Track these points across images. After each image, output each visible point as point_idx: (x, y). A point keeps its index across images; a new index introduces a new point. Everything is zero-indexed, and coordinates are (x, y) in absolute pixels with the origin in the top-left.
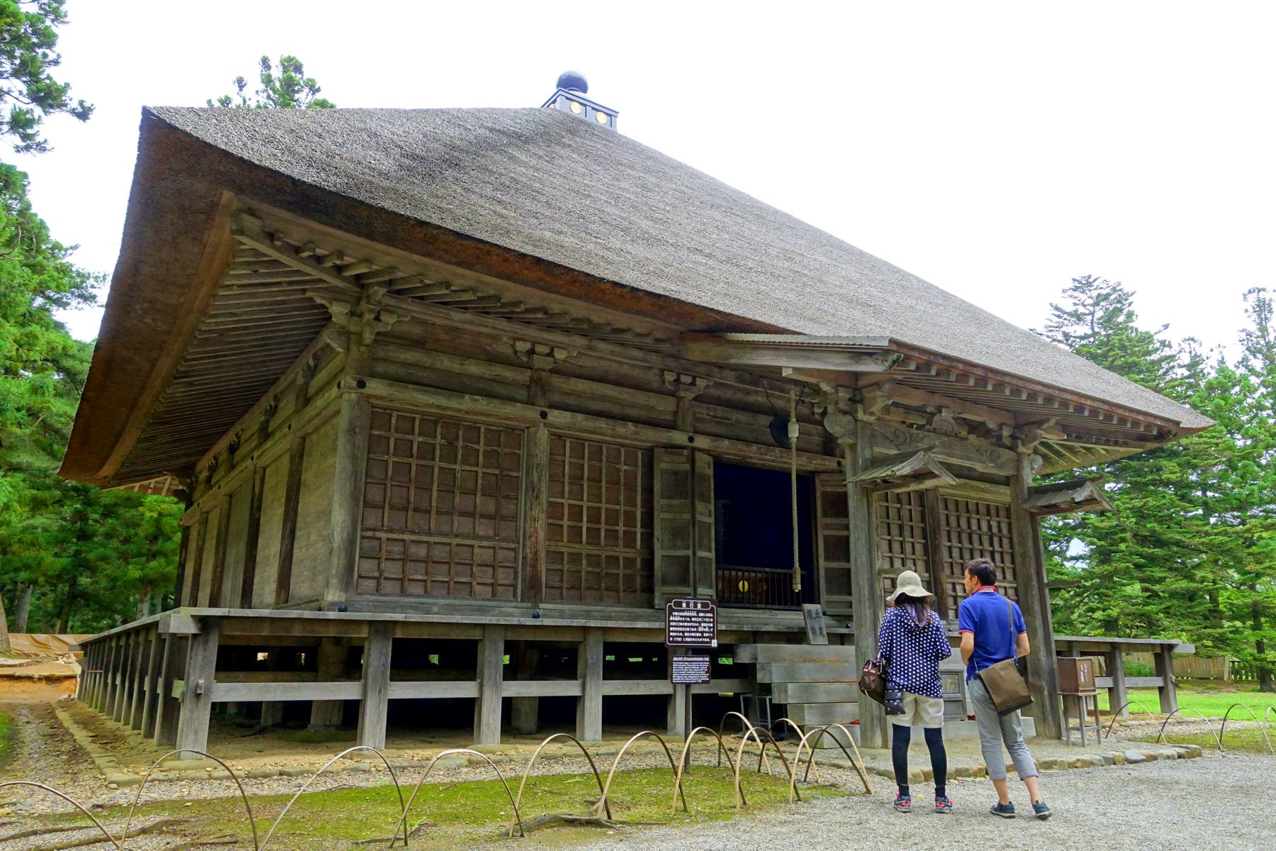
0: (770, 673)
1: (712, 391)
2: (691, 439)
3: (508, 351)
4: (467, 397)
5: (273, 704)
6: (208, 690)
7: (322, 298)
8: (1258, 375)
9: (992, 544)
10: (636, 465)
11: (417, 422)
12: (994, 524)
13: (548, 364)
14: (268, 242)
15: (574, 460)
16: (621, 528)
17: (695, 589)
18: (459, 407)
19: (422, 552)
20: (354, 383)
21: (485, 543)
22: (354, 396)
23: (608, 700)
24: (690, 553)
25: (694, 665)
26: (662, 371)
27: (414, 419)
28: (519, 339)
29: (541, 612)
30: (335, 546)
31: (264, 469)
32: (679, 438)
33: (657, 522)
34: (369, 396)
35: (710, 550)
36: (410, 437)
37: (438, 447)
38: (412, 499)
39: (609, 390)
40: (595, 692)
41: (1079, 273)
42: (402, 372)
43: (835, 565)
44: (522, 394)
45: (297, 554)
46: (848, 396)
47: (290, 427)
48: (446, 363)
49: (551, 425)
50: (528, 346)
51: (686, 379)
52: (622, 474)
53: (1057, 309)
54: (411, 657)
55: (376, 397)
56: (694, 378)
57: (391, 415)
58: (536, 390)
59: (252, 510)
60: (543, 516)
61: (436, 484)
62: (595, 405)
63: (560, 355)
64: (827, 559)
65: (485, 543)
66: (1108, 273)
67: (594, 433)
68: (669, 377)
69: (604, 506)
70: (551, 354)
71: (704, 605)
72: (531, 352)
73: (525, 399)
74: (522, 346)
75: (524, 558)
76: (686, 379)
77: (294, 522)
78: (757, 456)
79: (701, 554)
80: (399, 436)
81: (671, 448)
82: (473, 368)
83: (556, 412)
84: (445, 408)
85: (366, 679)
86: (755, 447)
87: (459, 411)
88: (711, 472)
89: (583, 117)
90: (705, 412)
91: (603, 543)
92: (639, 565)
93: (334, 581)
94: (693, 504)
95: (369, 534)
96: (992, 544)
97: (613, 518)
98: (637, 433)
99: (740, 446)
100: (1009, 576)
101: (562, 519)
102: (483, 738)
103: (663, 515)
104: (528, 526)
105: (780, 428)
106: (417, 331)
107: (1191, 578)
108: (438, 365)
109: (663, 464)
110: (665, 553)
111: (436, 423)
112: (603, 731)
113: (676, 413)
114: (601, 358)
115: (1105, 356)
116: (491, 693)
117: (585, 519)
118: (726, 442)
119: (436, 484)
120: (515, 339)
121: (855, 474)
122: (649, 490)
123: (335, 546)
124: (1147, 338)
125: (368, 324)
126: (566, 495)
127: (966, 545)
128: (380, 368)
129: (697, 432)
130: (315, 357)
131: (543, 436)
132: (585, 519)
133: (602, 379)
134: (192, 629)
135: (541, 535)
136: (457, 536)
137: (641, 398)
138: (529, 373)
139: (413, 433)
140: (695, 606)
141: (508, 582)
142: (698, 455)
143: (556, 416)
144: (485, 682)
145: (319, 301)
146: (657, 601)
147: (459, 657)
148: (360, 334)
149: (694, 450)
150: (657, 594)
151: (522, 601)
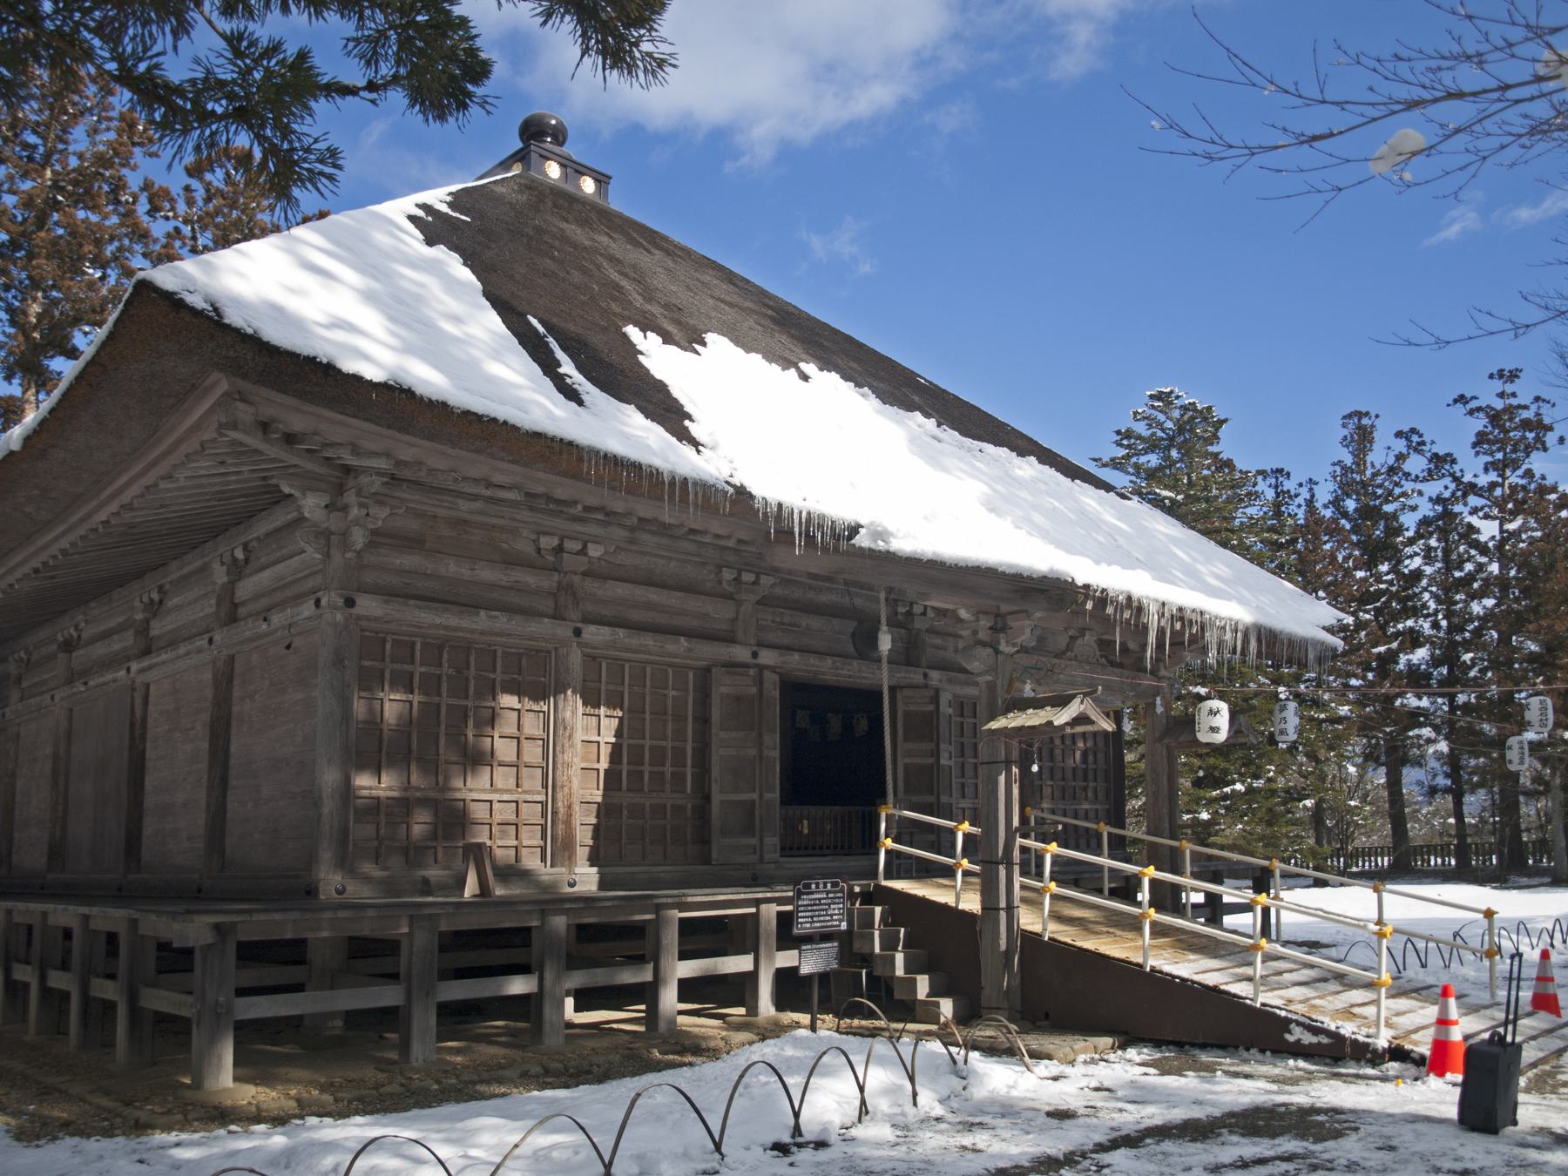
1: (778, 591)
2: (755, 655)
3: (530, 549)
4: (482, 613)
7: (291, 486)
10: (687, 690)
11: (418, 647)
13: (580, 563)
14: (260, 434)
15: (611, 687)
16: (668, 769)
17: (761, 839)
18: (474, 626)
20: (340, 602)
21: (506, 797)
22: (339, 617)
24: (755, 796)
26: (720, 567)
27: (414, 643)
28: (545, 533)
32: (741, 653)
33: (715, 760)
34: (359, 618)
36: (408, 667)
38: (414, 746)
39: (654, 595)
44: (547, 605)
46: (989, 625)
47: (211, 641)
48: (452, 568)
49: (586, 645)
50: (556, 542)
51: (748, 577)
52: (670, 702)
55: (368, 618)
56: (758, 575)
57: (384, 641)
58: (563, 601)
59: (132, 738)
61: (443, 727)
62: (636, 616)
63: (595, 551)
67: (636, 652)
68: (728, 575)
69: (648, 743)
70: (583, 552)
72: (559, 549)
73: (550, 611)
74: (548, 542)
76: (748, 577)
78: (832, 671)
79: (768, 796)
80: (396, 666)
81: (732, 666)
82: (487, 574)
84: (456, 629)
86: (829, 661)
87: (473, 631)
88: (776, 694)
90: (770, 617)
92: (689, 812)
94: (760, 735)
97: (659, 756)
98: (690, 650)
99: (813, 660)
100: (1101, 796)
103: (722, 752)
104: (559, 773)
105: (865, 641)
106: (413, 525)
108: (443, 571)
109: (723, 687)
110: (725, 797)
111: (441, 648)
113: (735, 620)
114: (642, 553)
117: (625, 760)
118: (796, 656)
120: (539, 533)
122: (703, 720)
125: (356, 522)
128: (369, 578)
129: (760, 644)
130: (246, 547)
132: (625, 760)
133: (649, 582)
134: (208, 938)
137: (693, 603)
138: (556, 577)
139: (413, 662)
141: (535, 843)
142: (767, 674)
143: (592, 633)
146: (714, 856)
148: (345, 534)
149: (761, 668)
150: (714, 847)
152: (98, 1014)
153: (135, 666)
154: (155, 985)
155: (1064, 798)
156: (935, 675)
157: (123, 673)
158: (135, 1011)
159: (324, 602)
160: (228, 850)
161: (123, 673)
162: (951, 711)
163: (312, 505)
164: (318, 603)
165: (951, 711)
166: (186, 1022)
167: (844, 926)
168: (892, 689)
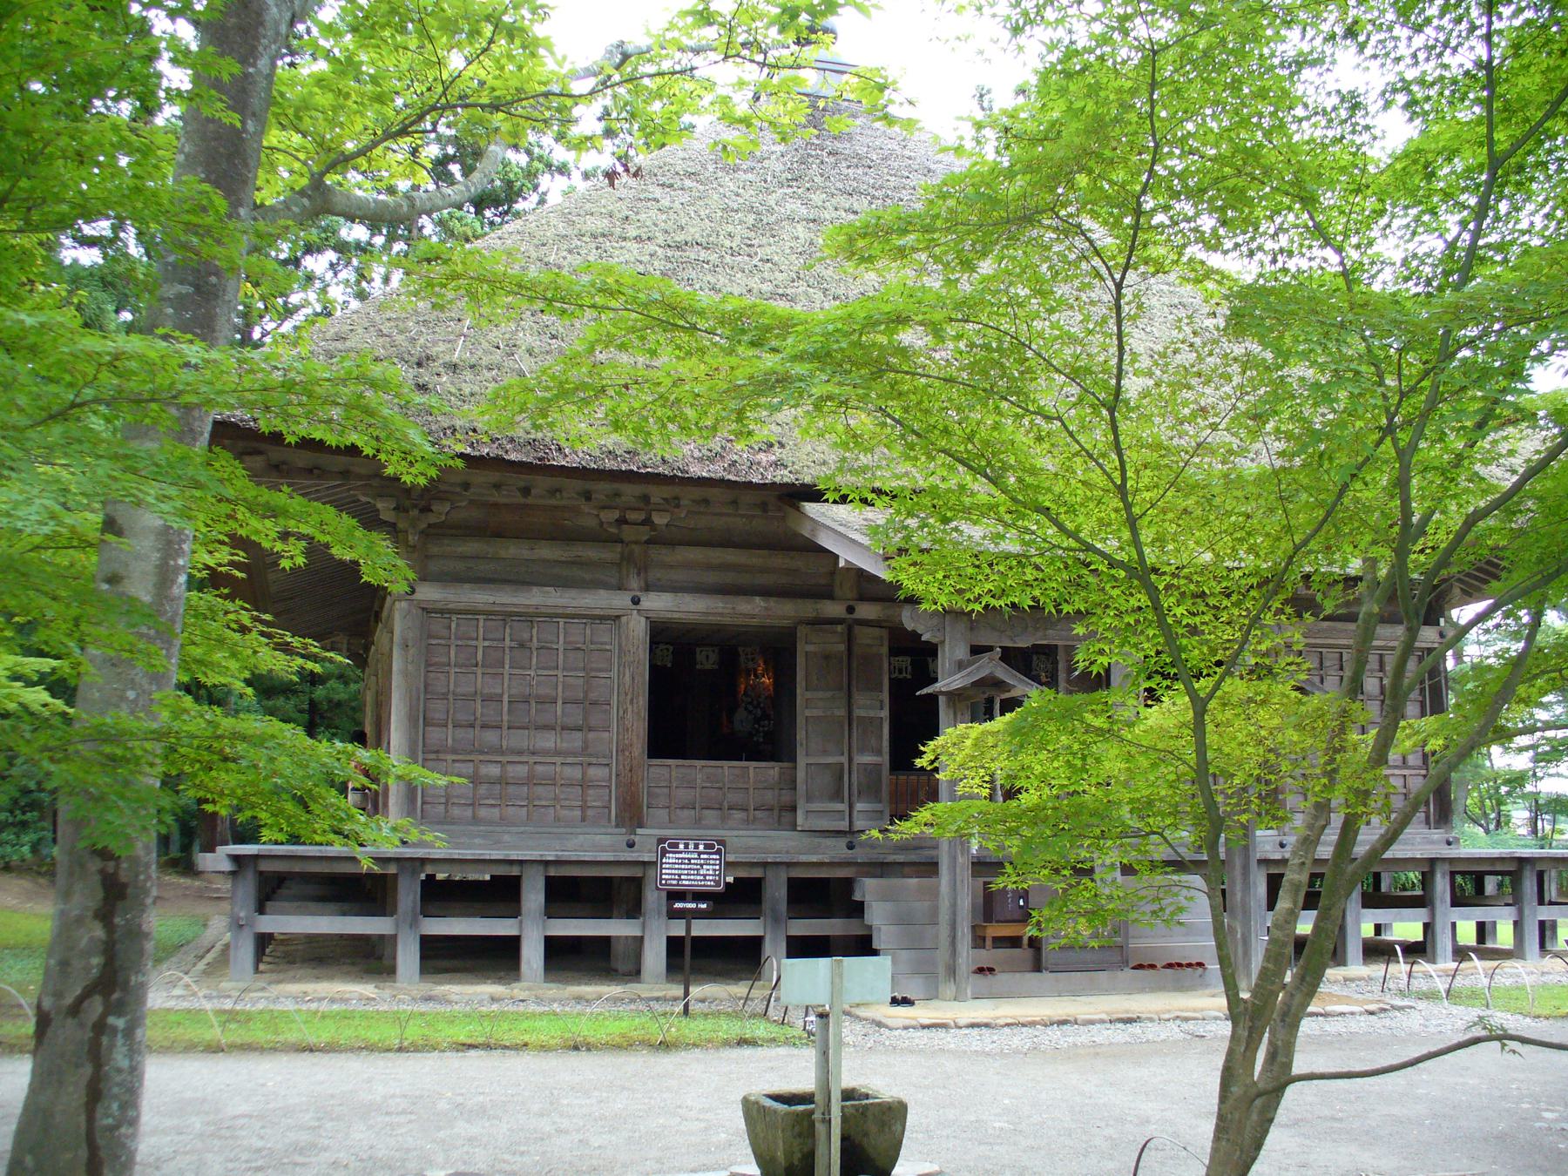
2: (851, 610)
3: (590, 523)
17: (851, 807)
19: (494, 770)
24: (844, 759)
32: (834, 609)
35: (879, 752)
40: (533, 929)
42: (460, 566)
50: (616, 514)
54: (442, 894)
71: (706, 846)
72: (622, 521)
83: (652, 595)
108: (503, 554)
116: (533, 929)
138: (619, 548)
140: (696, 846)
145: (364, 499)
146: (800, 821)
147: (500, 892)
151: (617, 826)
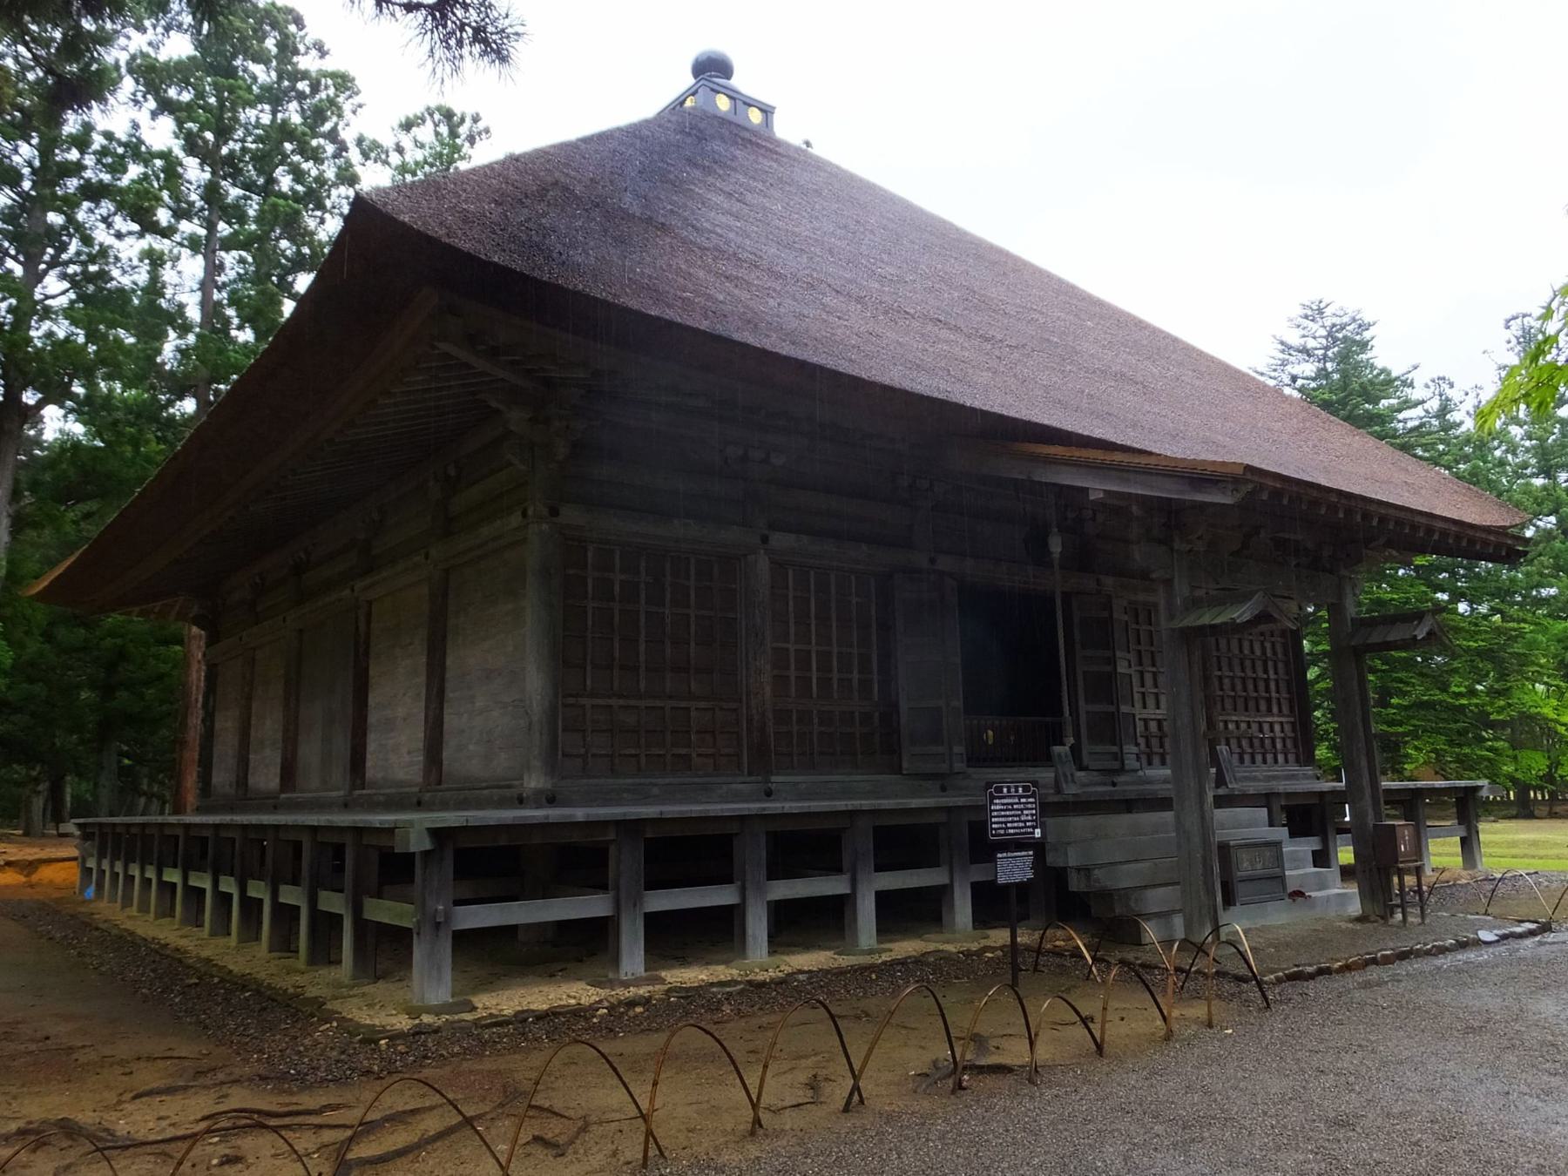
0: (1066, 854)
2: (932, 561)
5: (528, 926)
6: (448, 917)
8: (1520, 424)
9: (1266, 671)
12: (1268, 645)
21: (703, 705)
23: (883, 898)
25: (1019, 862)
29: (773, 787)
30: (535, 719)
31: (370, 603)
37: (642, 586)
41: (1311, 296)
43: (1098, 708)
45: (450, 720)
47: (427, 557)
53: (1282, 343)
60: (768, 667)
61: (643, 632)
64: (1087, 701)
65: (703, 705)
66: (1345, 301)
71: (1026, 789)
75: (750, 721)
77: (443, 680)
85: (617, 889)
89: (732, 117)
91: (835, 696)
93: (537, 763)
95: (571, 700)
96: (1266, 671)
100: (1285, 710)
101: (840, 680)
102: (750, 953)
105: (1038, 542)
107: (1444, 688)
112: (878, 931)
115: (1343, 403)
119: (643, 632)
121: (1172, 617)
123: (535, 719)
124: (1388, 383)
126: (792, 637)
127: (1250, 673)
131: (763, 564)
135: (768, 689)
136: (671, 697)
143: (780, 540)
144: (748, 885)
146: (905, 765)
151: (750, 774)
152: (326, 926)
153: (359, 585)
154: (379, 896)
155: (1246, 710)
156: (1109, 581)
157: (347, 592)
158: (361, 925)
159: (530, 512)
160: (445, 767)
161: (347, 592)
162: (1126, 618)
163: (516, 418)
164: (524, 515)
165: (1126, 618)
166: (410, 930)
167: (1038, 833)
168: (1066, 597)
